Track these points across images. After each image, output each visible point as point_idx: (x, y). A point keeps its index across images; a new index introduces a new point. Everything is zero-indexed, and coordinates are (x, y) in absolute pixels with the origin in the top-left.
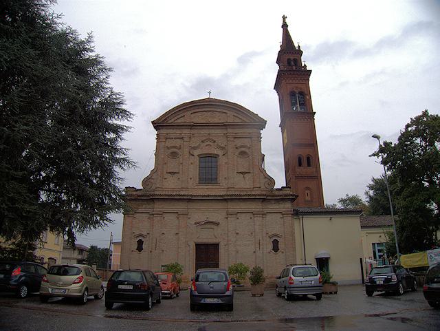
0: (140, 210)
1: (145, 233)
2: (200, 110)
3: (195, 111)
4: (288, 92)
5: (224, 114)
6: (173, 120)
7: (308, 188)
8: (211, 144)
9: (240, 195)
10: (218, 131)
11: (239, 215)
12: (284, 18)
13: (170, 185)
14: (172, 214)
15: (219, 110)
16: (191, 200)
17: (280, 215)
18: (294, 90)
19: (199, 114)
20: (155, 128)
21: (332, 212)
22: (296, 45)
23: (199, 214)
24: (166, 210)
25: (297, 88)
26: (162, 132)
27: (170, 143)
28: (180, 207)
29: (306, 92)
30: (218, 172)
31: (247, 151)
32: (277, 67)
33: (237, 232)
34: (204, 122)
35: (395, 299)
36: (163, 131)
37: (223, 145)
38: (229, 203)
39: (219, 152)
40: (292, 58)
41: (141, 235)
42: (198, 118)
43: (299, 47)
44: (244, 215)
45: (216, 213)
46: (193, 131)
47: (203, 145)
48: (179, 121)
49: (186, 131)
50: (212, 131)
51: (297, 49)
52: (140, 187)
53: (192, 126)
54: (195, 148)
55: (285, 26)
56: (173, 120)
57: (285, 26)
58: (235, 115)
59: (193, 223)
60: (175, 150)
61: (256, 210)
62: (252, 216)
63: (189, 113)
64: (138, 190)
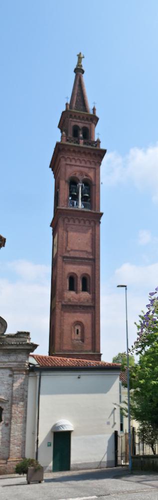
7: (78, 323)
12: (80, 58)
17: (8, 372)
22: (90, 106)
25: (81, 173)
29: (94, 183)
32: (57, 136)
40: (81, 125)
43: (94, 109)
55: (79, 71)
57: (79, 71)
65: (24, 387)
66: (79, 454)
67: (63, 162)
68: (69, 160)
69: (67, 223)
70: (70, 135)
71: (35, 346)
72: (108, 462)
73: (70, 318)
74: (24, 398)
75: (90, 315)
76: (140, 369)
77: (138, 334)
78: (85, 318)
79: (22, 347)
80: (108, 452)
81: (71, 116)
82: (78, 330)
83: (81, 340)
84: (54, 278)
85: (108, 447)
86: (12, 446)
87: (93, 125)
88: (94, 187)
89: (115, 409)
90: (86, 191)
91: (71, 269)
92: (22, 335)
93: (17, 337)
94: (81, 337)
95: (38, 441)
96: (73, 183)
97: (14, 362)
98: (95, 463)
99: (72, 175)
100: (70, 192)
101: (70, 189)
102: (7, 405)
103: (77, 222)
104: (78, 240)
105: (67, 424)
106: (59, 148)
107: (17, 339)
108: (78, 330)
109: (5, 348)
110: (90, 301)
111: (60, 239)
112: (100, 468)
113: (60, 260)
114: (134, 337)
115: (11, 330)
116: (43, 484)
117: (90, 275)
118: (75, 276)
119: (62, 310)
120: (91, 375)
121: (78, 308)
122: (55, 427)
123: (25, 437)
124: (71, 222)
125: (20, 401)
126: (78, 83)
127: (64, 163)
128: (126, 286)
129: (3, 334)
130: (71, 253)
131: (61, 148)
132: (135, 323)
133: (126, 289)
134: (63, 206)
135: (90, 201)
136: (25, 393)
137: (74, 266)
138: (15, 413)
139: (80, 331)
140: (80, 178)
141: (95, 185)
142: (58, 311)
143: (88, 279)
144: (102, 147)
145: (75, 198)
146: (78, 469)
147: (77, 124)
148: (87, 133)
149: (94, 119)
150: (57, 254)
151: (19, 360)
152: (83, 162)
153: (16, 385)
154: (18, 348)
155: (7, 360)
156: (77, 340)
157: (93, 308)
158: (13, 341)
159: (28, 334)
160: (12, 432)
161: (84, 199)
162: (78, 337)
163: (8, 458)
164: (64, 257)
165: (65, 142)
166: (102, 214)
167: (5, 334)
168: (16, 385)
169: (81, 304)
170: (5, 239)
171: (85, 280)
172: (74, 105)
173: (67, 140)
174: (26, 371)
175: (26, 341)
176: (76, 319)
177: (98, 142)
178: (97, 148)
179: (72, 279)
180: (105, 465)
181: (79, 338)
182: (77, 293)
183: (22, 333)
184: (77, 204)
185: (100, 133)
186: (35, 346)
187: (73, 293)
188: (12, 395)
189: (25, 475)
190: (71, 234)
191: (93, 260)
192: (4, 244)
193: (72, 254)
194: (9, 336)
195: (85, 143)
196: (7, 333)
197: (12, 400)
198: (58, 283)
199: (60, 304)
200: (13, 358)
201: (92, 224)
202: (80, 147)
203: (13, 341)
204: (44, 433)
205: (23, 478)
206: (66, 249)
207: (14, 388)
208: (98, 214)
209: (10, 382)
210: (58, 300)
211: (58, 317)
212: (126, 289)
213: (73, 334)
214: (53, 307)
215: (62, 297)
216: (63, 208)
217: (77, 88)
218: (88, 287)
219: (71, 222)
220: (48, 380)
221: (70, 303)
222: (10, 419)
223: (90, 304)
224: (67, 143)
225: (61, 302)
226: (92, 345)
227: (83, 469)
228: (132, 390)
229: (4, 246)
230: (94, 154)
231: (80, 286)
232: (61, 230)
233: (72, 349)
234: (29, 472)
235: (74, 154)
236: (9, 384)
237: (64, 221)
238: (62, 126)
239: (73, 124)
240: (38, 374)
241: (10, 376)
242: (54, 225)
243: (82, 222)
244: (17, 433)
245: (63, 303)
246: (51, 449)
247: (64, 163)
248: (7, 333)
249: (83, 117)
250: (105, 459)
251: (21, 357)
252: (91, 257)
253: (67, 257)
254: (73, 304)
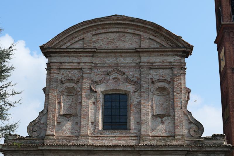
69: (232, 37)
71: (4, 140)
79: (221, 149)
84: (224, 90)
92: (218, 138)
93: (215, 140)
107: (215, 142)
109: (204, 150)
111: (228, 52)
129: (200, 137)
134: (227, 22)
150: (226, 66)
154: (216, 150)
158: (211, 143)
166: (186, 63)
167: (202, 137)
170: (193, 47)
175: (223, 143)
186: (4, 140)
192: (191, 52)
194: (206, 139)
196: (204, 135)
203: (211, 143)
208: (184, 63)
214: (225, 117)
216: (228, 23)
229: (191, 55)
237: (229, 35)
248: (204, 135)
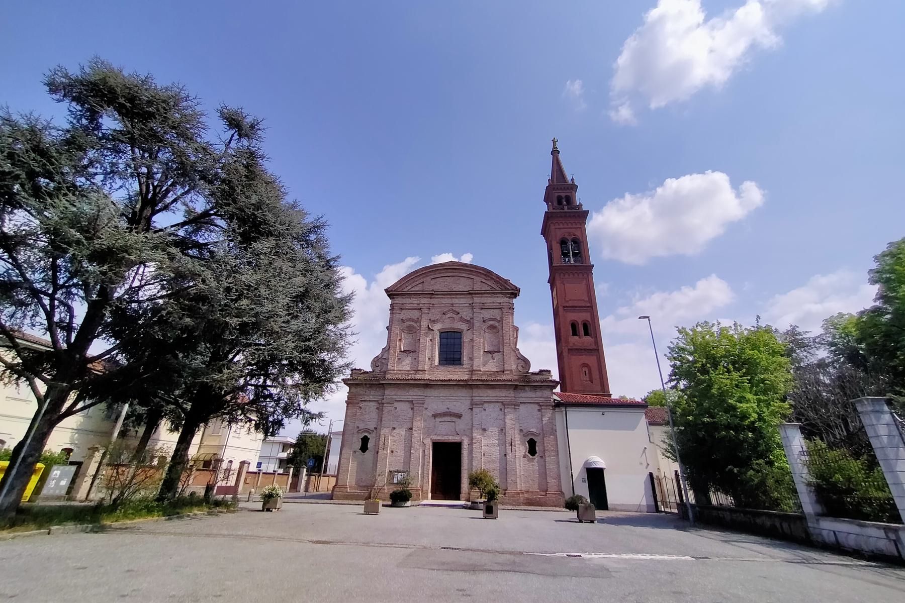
0: (367, 398)
1: (372, 427)
2: (442, 275)
3: (435, 276)
4: (558, 241)
5: (470, 280)
6: (410, 287)
7: (585, 365)
8: (454, 316)
9: (487, 381)
10: (463, 301)
11: (486, 405)
12: (554, 142)
13: (400, 368)
14: (532, 405)
15: (464, 275)
16: (428, 385)
17: (537, 407)
18: (566, 236)
19: (441, 279)
20: (389, 296)
21: (625, 405)
22: (569, 178)
23: (437, 401)
24: (486, 399)
25: (570, 234)
26: (397, 302)
27: (405, 315)
28: (414, 394)
29: (581, 241)
30: (462, 351)
31: (497, 324)
32: (544, 208)
33: (483, 427)
34: (447, 290)
35: (810, 567)
36: (399, 300)
37: (468, 318)
38: (475, 390)
39: (463, 326)
40: (563, 195)
41: (367, 430)
42: (440, 285)
43: (572, 180)
44: (492, 405)
45: (459, 402)
46: (434, 301)
47: (444, 317)
48: (417, 289)
49: (424, 300)
50: (455, 301)
51: (570, 182)
52: (368, 368)
53: (432, 295)
54: (434, 322)
55: (555, 152)
56: (410, 287)
57: (555, 152)
58: (483, 281)
59: (430, 414)
60: (412, 323)
61: (508, 400)
62: (502, 407)
63: (428, 278)
64: (366, 373)
65: (552, 420)
66: (614, 493)
67: (552, 227)
68: (557, 224)
70: (555, 204)
72: (648, 506)
73: (576, 361)
74: (554, 432)
75: (595, 357)
76: (686, 404)
77: (671, 366)
78: (591, 360)
79: (546, 384)
80: (646, 494)
81: (554, 189)
82: (585, 372)
83: (590, 381)
84: (557, 326)
85: (645, 489)
86: (548, 478)
87: (574, 192)
88: (582, 244)
89: (646, 448)
90: (576, 248)
91: (573, 316)
92: (544, 373)
94: (590, 378)
95: (572, 475)
96: (563, 242)
97: (541, 397)
98: (634, 505)
99: (561, 237)
100: (562, 251)
101: (561, 248)
102: (539, 438)
103: (571, 276)
104: (574, 290)
105: (599, 462)
106: (548, 217)
107: (541, 377)
108: (585, 372)
110: (593, 345)
112: (640, 512)
113: (561, 309)
114: (667, 370)
115: (534, 369)
116: (596, 525)
117: (590, 320)
118: (576, 323)
119: (568, 353)
120: (30, 536)
121: (583, 351)
122: (586, 463)
123: (559, 470)
124: (567, 276)
125: (551, 435)
126: (555, 162)
127: (554, 227)
128: (648, 317)
130: (570, 302)
131: (550, 216)
132: (665, 355)
133: (649, 320)
135: (580, 257)
136: (554, 427)
137: (574, 314)
138: (548, 446)
139: (587, 372)
140: (570, 238)
141: (583, 242)
142: (565, 354)
143: (589, 326)
144: (584, 208)
145: (566, 255)
146: (617, 510)
147: (560, 194)
148: (569, 200)
149: (574, 187)
151: (545, 396)
152: (569, 224)
153: (545, 419)
155: (534, 396)
156: (586, 381)
157: (597, 351)
158: (538, 378)
159: (550, 371)
160: (547, 465)
161: (575, 255)
162: (587, 377)
163: (547, 491)
164: (564, 307)
165: (551, 210)
168: (545, 419)
169: (585, 348)
171: (585, 326)
172: (555, 180)
173: (554, 209)
174: (552, 406)
176: (582, 362)
177: (581, 205)
178: (580, 210)
179: (574, 326)
180: (646, 509)
181: (588, 379)
182: (580, 338)
183: (544, 371)
184: (569, 261)
185: (580, 197)
187: (576, 337)
188: (543, 429)
189: (576, 511)
190: (567, 285)
191: (591, 307)
193: (570, 304)
194: (533, 374)
195: (568, 209)
196: (531, 371)
197: (543, 434)
198: (562, 330)
199: (567, 348)
200: (539, 393)
201: (585, 275)
202: (566, 212)
203: (538, 378)
204: (578, 470)
205: (573, 515)
206: (565, 299)
207: (544, 422)
209: (539, 416)
210: (564, 344)
211: (566, 359)
212: (649, 320)
213: (582, 375)
215: (567, 342)
217: (555, 165)
218: (589, 332)
219: (567, 276)
220: (574, 415)
221: (575, 347)
222: (544, 452)
223: (593, 347)
224: (554, 211)
225: (567, 346)
226: (601, 386)
227: (621, 511)
228: (675, 429)
230: (578, 216)
231: (582, 332)
232: (558, 283)
233: (582, 389)
234: (580, 509)
235: (561, 219)
236: (538, 419)
238: (546, 200)
239: (557, 195)
240: (563, 409)
241: (539, 410)
242: (552, 281)
243: (576, 275)
244: (551, 467)
245: (569, 347)
246: (586, 484)
247: (554, 227)
248: (531, 371)
249: (564, 188)
250: (644, 503)
251: (547, 393)
252: (589, 305)
253: (567, 307)
254: (578, 348)
